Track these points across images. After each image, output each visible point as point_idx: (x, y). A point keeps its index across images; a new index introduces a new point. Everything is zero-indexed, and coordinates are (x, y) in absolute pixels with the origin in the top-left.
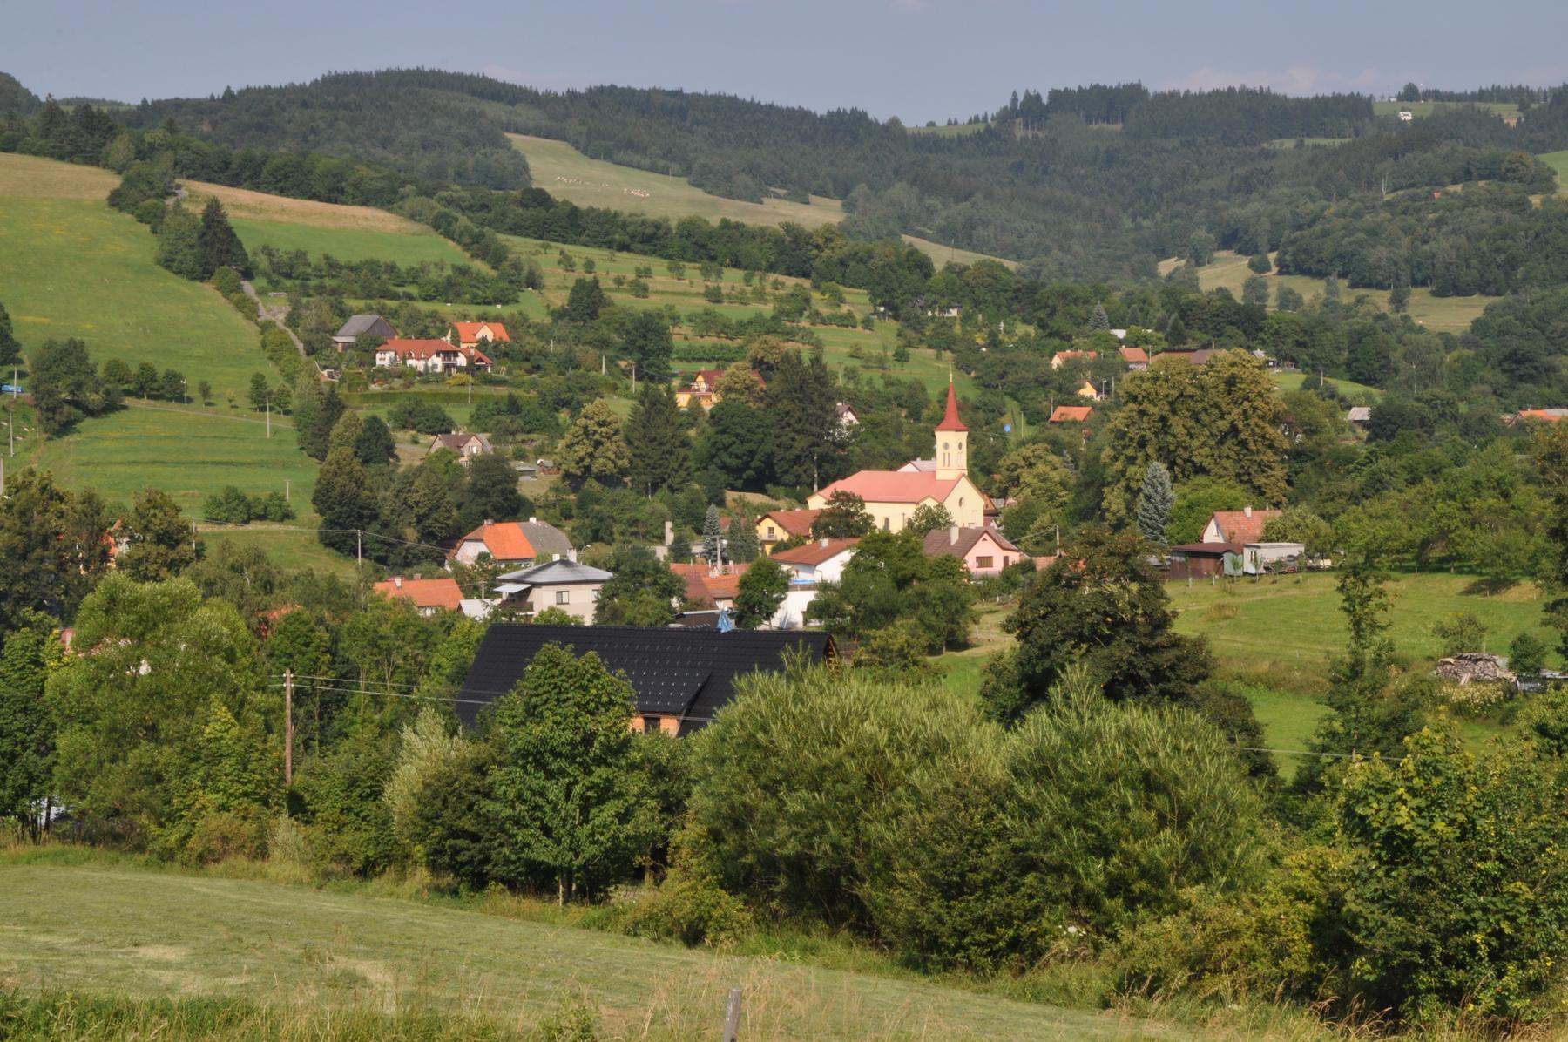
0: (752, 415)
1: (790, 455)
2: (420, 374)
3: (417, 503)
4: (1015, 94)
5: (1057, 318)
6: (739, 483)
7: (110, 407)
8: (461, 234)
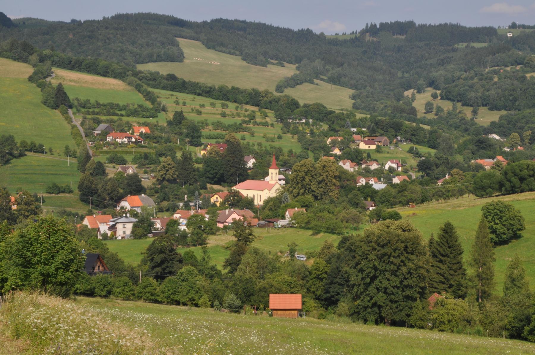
0: (217, 161)
1: (229, 173)
2: (120, 144)
3: (108, 189)
4: (367, 24)
5: (334, 125)
6: (213, 182)
7: (21, 155)
8: (143, 91)
